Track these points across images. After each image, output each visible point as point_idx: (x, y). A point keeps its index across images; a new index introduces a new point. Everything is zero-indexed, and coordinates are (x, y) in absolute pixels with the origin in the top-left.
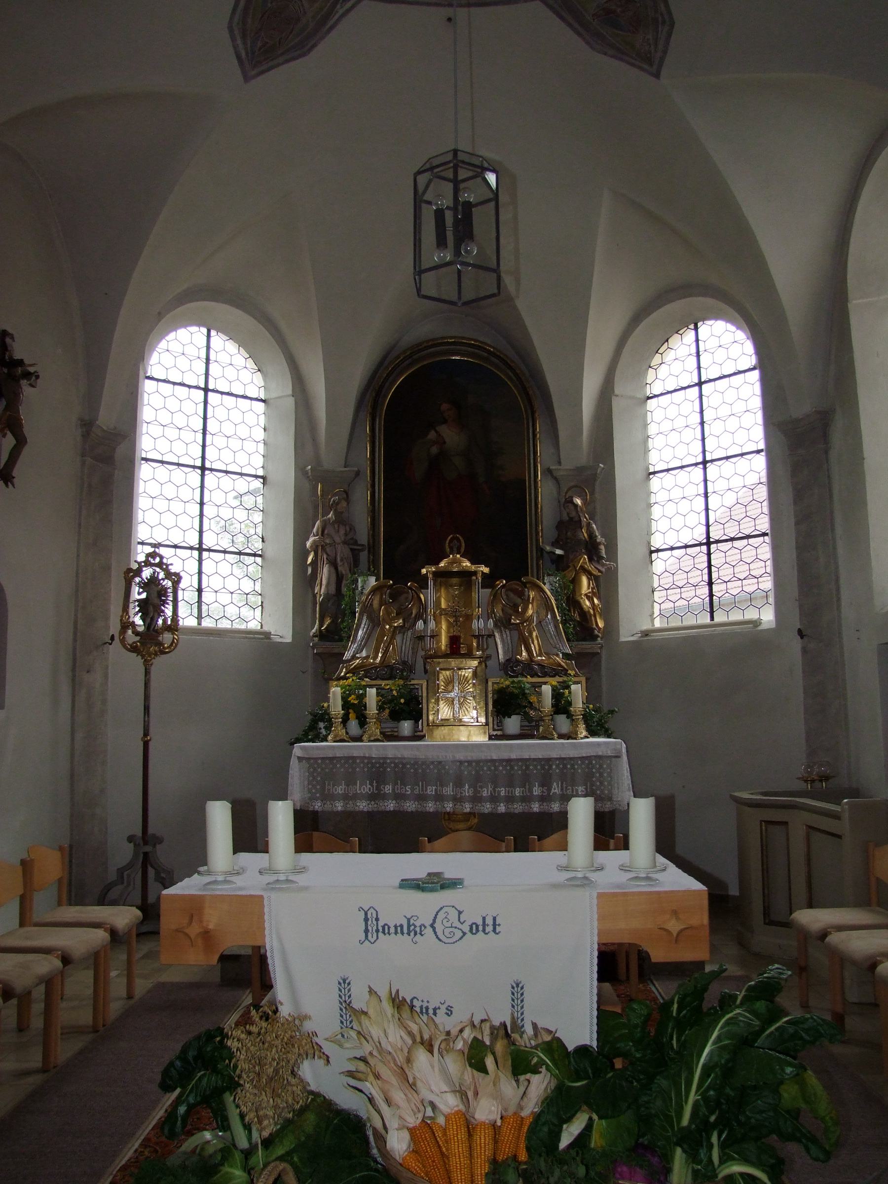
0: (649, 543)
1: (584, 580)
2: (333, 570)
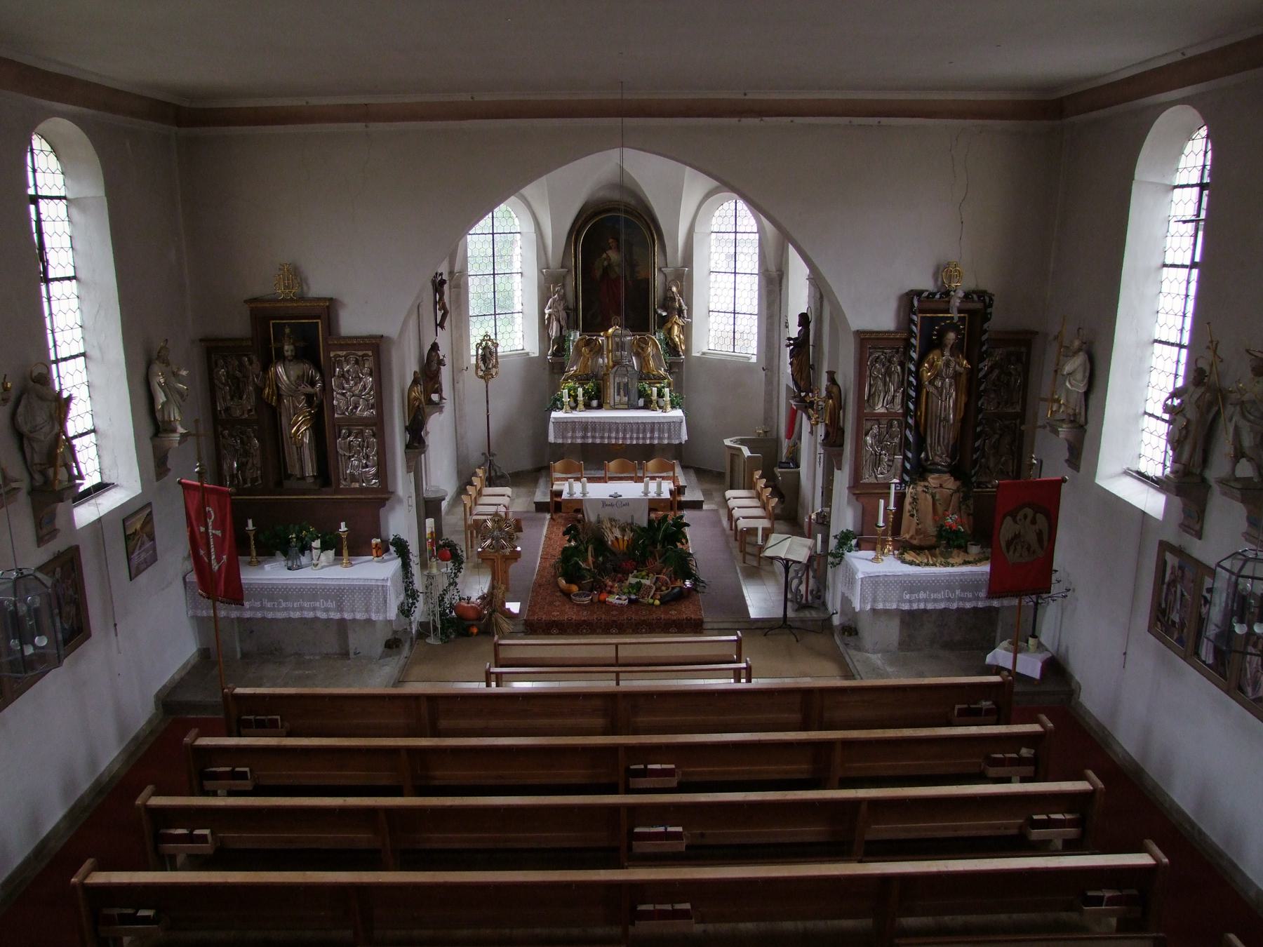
0: (709, 308)
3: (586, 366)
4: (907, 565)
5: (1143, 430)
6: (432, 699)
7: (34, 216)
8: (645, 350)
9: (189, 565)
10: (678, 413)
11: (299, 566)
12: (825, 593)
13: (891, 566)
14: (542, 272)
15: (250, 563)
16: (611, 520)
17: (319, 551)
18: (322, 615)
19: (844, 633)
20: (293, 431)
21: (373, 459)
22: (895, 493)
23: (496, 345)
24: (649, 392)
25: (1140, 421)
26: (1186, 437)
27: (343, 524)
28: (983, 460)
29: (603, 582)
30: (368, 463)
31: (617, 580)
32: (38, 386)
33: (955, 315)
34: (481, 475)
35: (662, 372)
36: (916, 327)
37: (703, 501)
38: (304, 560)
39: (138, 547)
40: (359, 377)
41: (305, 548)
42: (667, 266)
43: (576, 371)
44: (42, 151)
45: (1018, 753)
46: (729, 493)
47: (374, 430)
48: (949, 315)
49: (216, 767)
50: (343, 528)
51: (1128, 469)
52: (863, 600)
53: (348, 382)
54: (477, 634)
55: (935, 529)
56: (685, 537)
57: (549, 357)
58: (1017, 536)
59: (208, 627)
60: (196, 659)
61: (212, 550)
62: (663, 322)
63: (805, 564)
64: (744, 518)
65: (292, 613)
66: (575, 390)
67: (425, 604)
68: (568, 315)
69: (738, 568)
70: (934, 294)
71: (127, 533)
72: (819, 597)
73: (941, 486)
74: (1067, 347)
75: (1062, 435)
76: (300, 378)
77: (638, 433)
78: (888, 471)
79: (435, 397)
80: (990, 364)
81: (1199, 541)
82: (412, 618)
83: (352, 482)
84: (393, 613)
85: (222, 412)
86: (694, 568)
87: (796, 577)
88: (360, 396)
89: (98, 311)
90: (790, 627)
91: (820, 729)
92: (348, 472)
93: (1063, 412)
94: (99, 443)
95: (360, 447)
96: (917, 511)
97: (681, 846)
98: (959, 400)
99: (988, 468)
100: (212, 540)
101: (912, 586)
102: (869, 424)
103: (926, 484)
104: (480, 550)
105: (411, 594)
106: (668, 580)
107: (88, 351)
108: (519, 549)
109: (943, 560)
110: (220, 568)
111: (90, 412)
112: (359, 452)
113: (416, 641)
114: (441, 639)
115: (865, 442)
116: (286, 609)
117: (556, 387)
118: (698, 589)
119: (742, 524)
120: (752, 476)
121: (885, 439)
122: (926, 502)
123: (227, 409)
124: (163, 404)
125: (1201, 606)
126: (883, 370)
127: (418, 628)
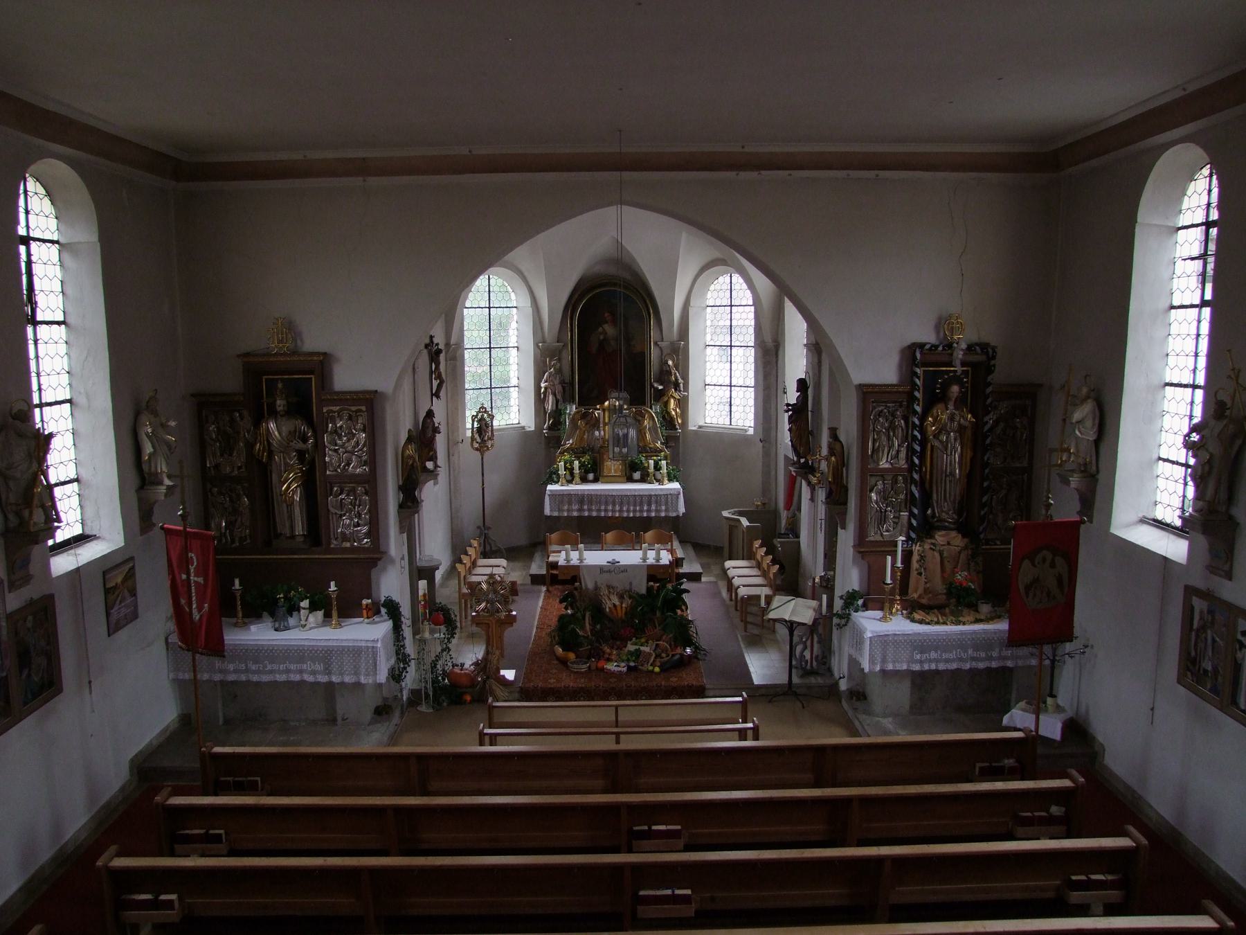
0: (705, 381)
1: (672, 401)
2: (554, 398)
3: (582, 439)
4: (917, 624)
5: (1158, 476)
6: (420, 757)
7: (24, 257)
8: (641, 423)
9: (172, 626)
10: (676, 485)
11: (286, 627)
12: (830, 661)
13: (900, 625)
14: (538, 346)
15: (236, 625)
16: (609, 587)
17: (307, 611)
18: (309, 678)
19: (852, 698)
20: (283, 488)
21: (365, 517)
22: (902, 551)
23: (492, 417)
24: (646, 465)
25: (1155, 467)
26: (1209, 473)
27: (333, 584)
28: (991, 516)
29: (601, 649)
30: (360, 522)
31: (615, 647)
32: (18, 423)
33: (959, 369)
34: (475, 545)
35: (659, 445)
36: (919, 380)
37: (701, 573)
38: (292, 621)
39: (118, 602)
40: (352, 432)
41: (293, 609)
42: (662, 341)
43: (572, 444)
44: (36, 193)
45: (1047, 811)
46: (728, 564)
47: (367, 487)
48: (952, 369)
49: (188, 829)
50: (333, 587)
51: (1144, 517)
52: (872, 661)
53: (340, 438)
54: (471, 702)
55: (944, 586)
56: (685, 604)
57: (544, 431)
58: (1036, 580)
59: (190, 690)
60: (176, 725)
61: (194, 598)
62: (659, 395)
63: (809, 626)
64: (744, 586)
65: (278, 676)
66: (572, 463)
67: (416, 671)
68: (564, 388)
69: (739, 636)
70: (936, 347)
71: (107, 587)
72: (824, 660)
73: (949, 544)
74: (1074, 396)
75: (1073, 485)
76: (293, 434)
77: (635, 505)
78: (894, 529)
79: (430, 465)
80: (995, 418)
81: (1230, 582)
82: (403, 684)
83: (342, 542)
84: (382, 676)
85: (212, 468)
86: (695, 635)
87: (801, 642)
88: (352, 453)
89: (87, 357)
90: (796, 694)
91: (834, 786)
92: (339, 531)
93: (1073, 461)
94: (82, 492)
95: (351, 505)
96: (925, 569)
97: (689, 911)
98: (964, 454)
99: (996, 524)
100: (193, 588)
101: (921, 645)
102: (873, 480)
103: (933, 541)
104: (474, 614)
105: (402, 658)
106: (668, 647)
107: (75, 397)
108: (514, 613)
109: (954, 619)
110: (201, 616)
111: (74, 461)
112: (350, 511)
113: (406, 709)
114: (433, 707)
115: (871, 497)
116: (271, 672)
117: (552, 461)
118: (699, 657)
119: (743, 592)
120: (751, 545)
121: (890, 496)
122: (934, 560)
123: (217, 466)
124: (150, 455)
125: (1236, 651)
126: (886, 425)
127: (409, 695)
